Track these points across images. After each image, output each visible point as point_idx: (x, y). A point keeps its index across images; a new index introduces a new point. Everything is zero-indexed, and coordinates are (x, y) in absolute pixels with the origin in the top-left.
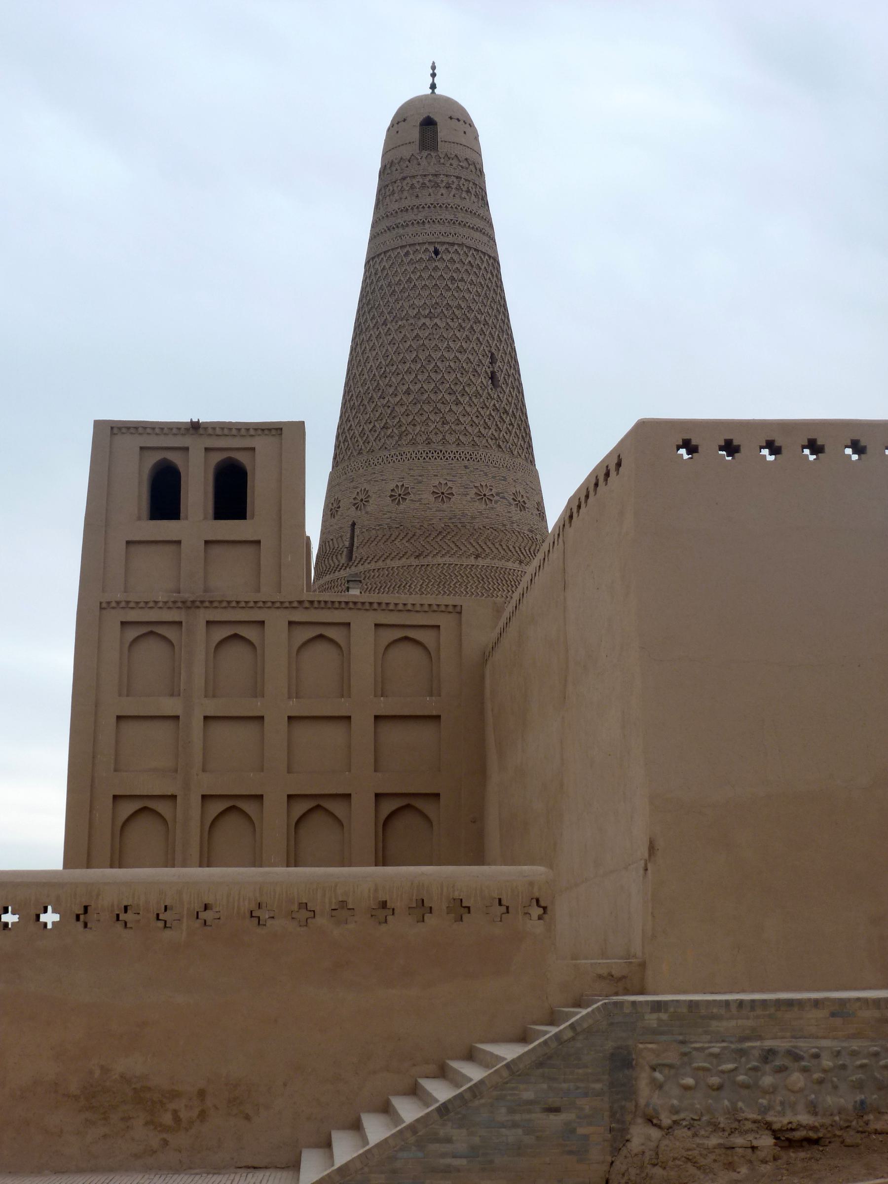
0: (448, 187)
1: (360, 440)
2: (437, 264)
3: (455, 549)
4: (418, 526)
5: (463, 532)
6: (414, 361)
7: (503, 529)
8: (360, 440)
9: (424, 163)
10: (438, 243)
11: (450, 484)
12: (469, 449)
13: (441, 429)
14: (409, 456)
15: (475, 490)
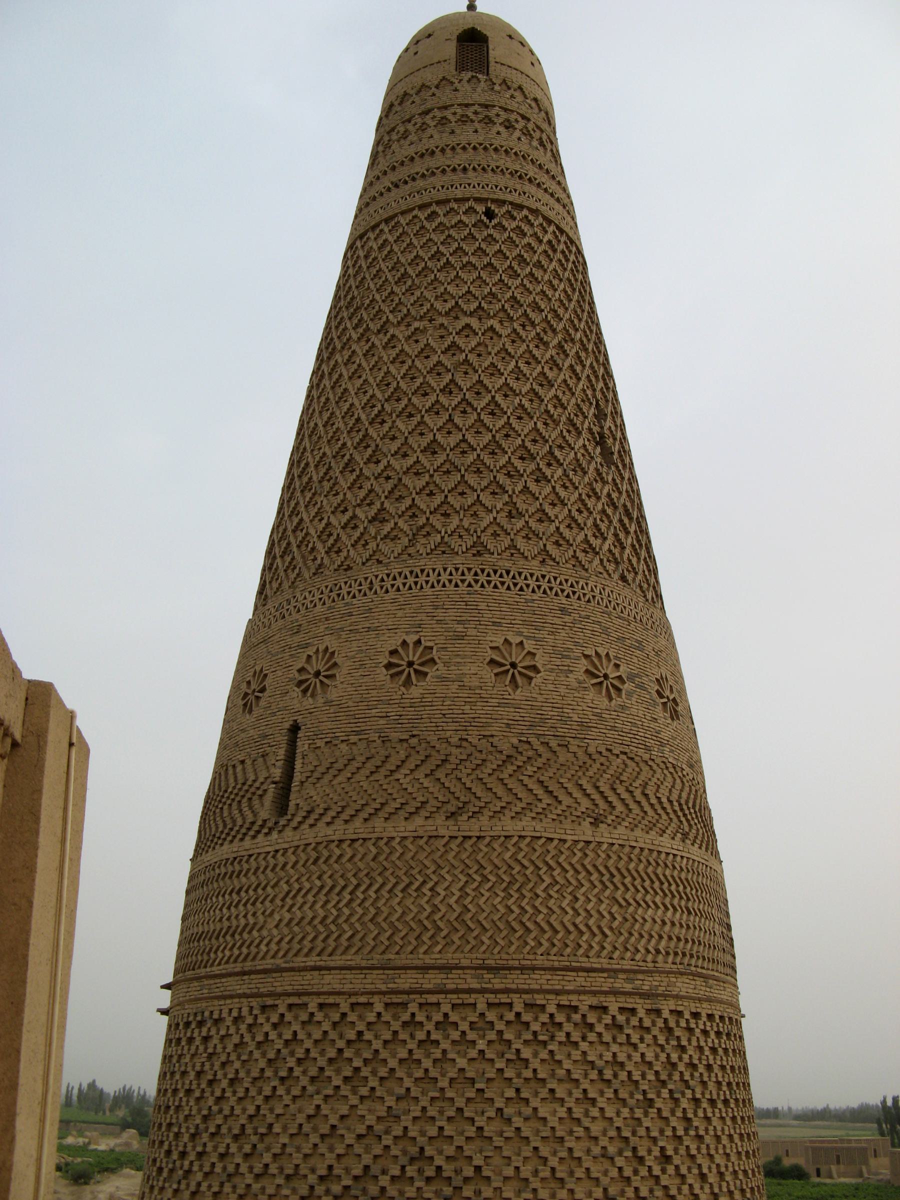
0: (509, 125)
1: (319, 546)
2: (491, 231)
3: (547, 800)
4: (454, 740)
5: (562, 760)
6: (447, 390)
7: (646, 757)
8: (319, 546)
9: (465, 87)
10: (494, 201)
11: (529, 646)
12: (567, 571)
13: (508, 527)
14: (433, 578)
15: (584, 664)
